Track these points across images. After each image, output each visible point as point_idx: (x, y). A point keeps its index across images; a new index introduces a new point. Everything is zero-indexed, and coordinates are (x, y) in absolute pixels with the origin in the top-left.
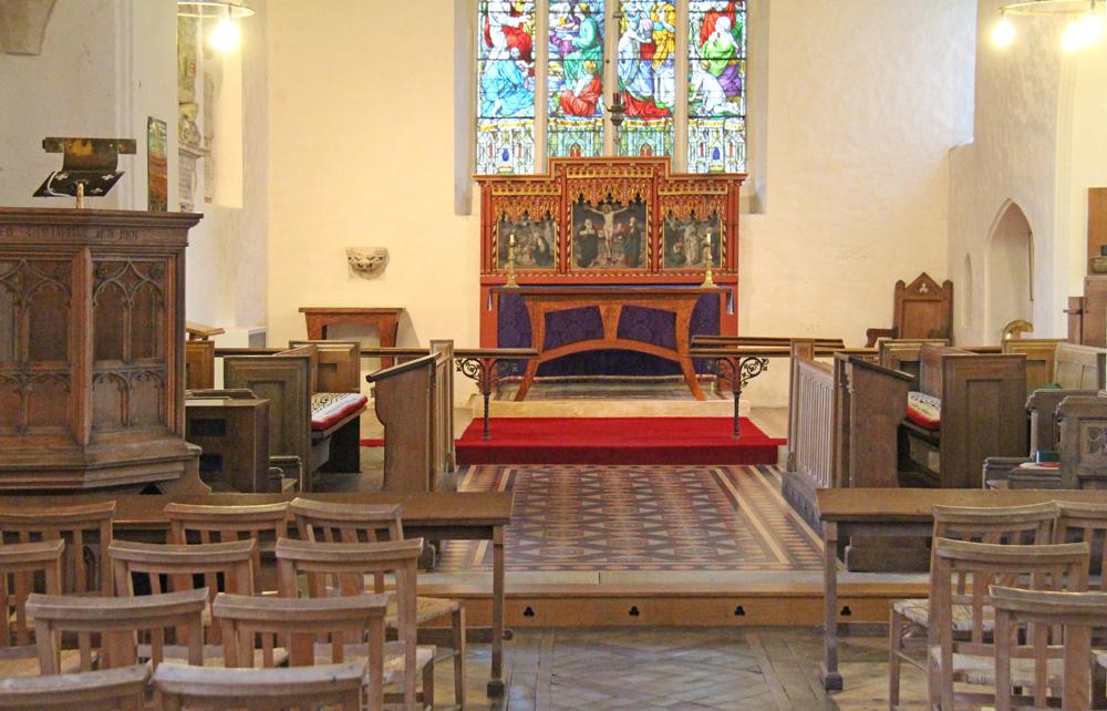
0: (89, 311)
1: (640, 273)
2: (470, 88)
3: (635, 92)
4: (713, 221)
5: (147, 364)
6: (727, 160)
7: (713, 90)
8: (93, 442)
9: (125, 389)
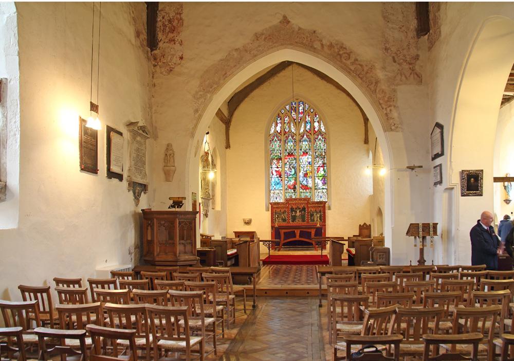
0: (178, 231)
1: (305, 223)
2: (269, 184)
4: (320, 212)
5: (189, 241)
7: (319, 182)
8: (179, 256)
9: (185, 246)
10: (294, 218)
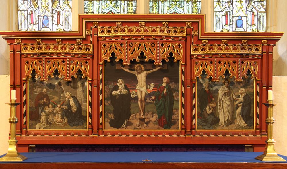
4: (247, 82)
10: (122, 110)
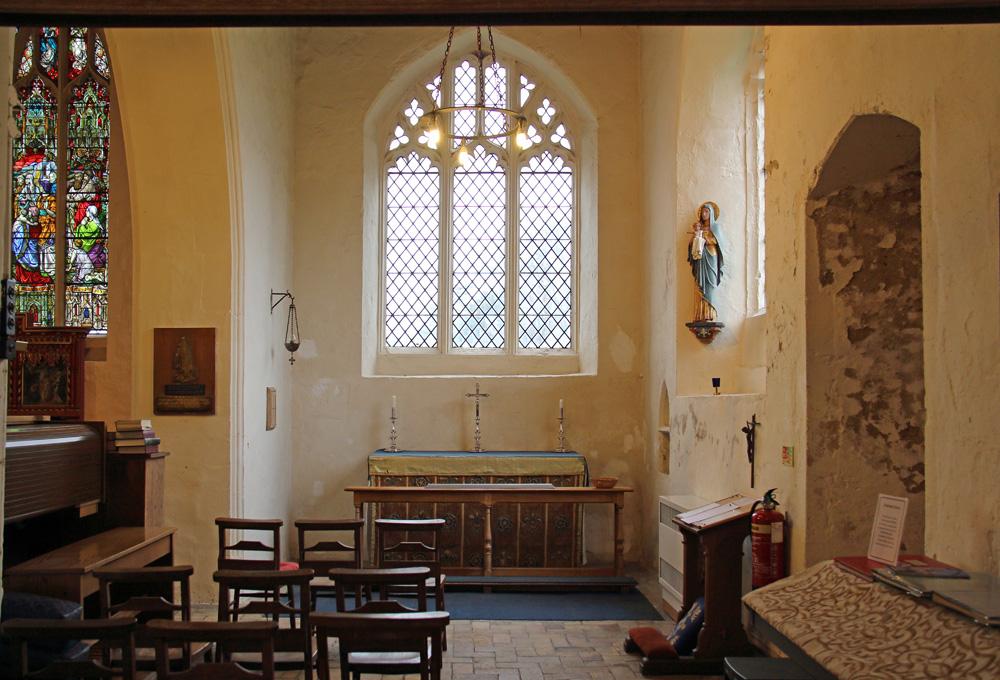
3: (25, 263)
4: (60, 365)
6: (95, 317)
7: (80, 256)
